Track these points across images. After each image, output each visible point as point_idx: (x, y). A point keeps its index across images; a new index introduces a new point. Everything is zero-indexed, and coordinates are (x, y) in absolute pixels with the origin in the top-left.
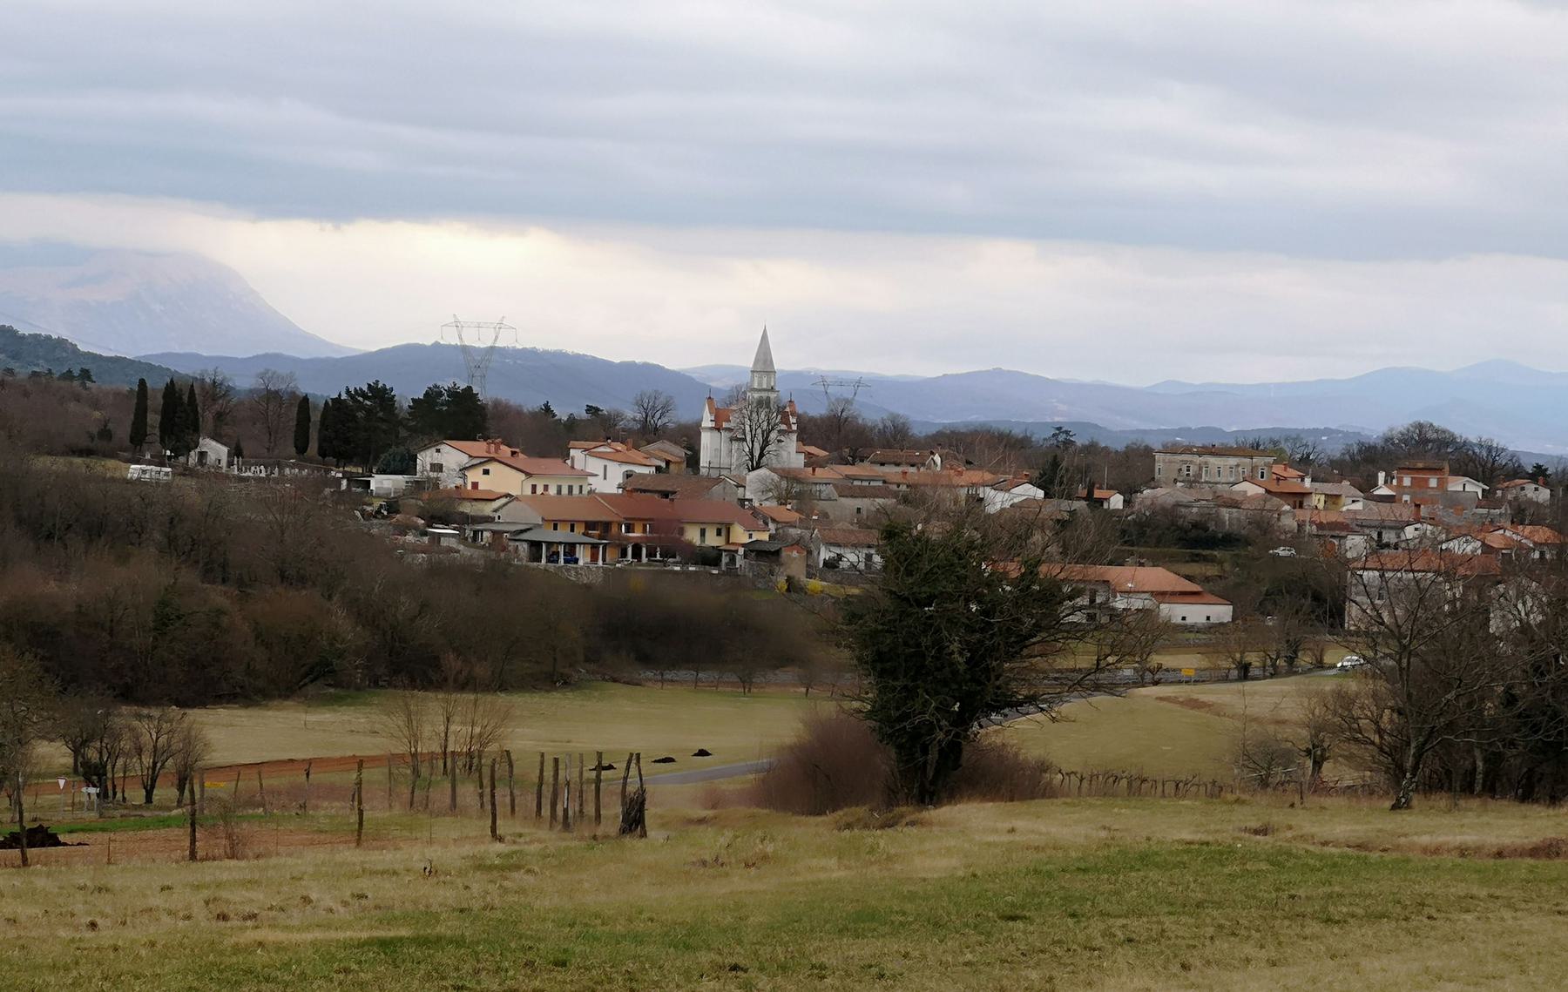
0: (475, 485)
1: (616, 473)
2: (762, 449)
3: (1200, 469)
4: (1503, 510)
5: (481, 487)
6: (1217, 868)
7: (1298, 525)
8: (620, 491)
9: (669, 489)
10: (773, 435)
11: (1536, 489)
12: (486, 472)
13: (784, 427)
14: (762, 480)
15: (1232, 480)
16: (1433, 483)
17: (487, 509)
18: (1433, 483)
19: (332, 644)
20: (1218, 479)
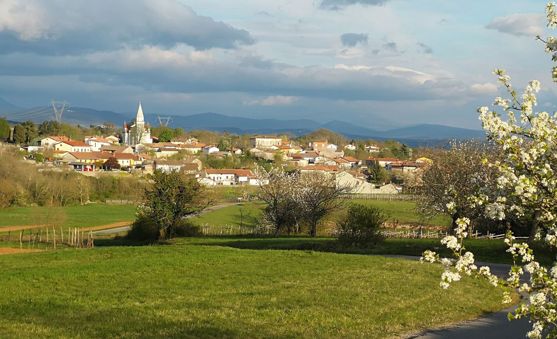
0: (58, 149)
1: (99, 145)
2: (140, 138)
3: (262, 142)
4: (342, 153)
5: (60, 150)
6: (413, 300)
7: (67, 214)
8: (100, 150)
9: (113, 150)
10: (143, 134)
11: (352, 147)
12: (61, 145)
13: (146, 132)
14: (140, 147)
15: (270, 145)
16: (323, 145)
17: (61, 155)
18: (323, 145)
19: (541, 224)
20: (267, 145)
